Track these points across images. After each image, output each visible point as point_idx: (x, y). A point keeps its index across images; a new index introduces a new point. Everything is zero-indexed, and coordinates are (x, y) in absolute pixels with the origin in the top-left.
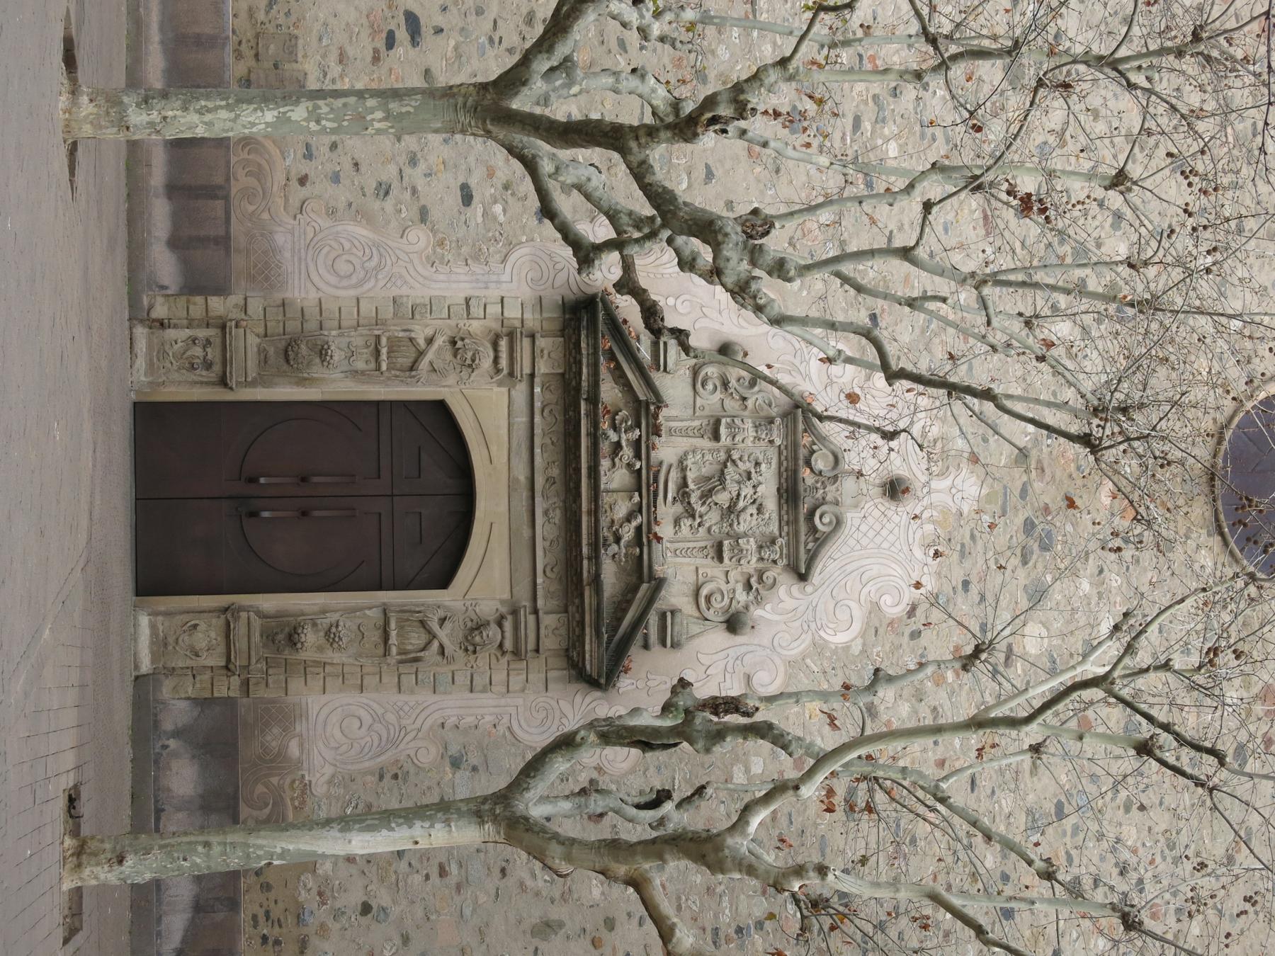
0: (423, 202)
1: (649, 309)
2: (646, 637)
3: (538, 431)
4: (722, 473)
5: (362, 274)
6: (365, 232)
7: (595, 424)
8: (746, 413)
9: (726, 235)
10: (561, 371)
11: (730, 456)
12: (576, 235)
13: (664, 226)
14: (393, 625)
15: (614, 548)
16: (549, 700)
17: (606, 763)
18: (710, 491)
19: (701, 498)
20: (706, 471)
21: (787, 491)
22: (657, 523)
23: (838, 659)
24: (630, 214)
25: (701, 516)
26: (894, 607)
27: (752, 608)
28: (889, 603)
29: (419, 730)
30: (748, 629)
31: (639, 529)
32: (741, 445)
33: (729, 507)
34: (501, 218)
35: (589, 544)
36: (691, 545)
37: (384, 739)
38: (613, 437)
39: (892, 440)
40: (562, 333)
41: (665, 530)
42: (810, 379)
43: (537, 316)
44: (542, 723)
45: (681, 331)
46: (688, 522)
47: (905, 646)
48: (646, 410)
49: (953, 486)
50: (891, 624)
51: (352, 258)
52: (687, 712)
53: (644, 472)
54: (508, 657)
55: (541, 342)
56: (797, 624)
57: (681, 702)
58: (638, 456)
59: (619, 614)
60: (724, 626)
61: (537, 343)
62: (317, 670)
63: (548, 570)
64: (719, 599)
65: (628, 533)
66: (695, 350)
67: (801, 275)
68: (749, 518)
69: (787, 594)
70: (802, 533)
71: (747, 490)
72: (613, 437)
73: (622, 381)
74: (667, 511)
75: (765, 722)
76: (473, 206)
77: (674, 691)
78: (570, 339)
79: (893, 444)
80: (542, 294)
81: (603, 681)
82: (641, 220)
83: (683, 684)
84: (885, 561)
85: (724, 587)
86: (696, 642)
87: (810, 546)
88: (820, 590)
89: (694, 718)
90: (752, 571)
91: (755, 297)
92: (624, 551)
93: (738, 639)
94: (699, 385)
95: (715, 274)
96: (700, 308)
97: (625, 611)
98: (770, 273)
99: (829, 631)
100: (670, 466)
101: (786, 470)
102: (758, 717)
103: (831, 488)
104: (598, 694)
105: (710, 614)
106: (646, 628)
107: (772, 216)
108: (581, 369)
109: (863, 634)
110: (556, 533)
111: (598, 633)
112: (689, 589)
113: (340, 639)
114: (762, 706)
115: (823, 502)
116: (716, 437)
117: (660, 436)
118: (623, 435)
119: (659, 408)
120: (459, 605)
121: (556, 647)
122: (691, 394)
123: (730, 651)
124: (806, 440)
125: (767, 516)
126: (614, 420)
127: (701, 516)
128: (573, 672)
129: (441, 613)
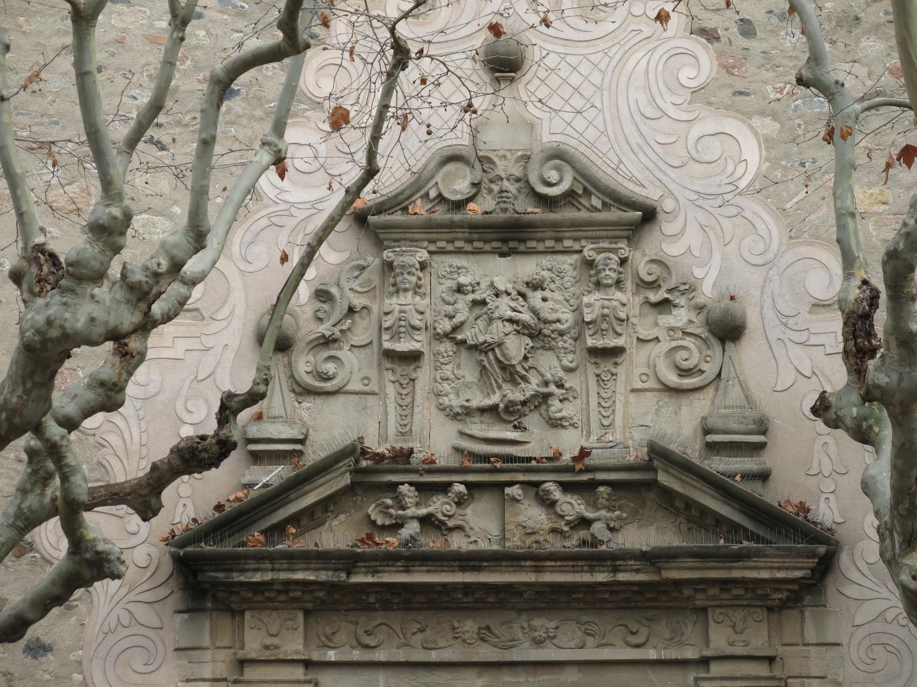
1: (185, 461)
2: (748, 476)
3: (401, 656)
4: (474, 348)
7: (390, 559)
8: (375, 308)
9: (49, 322)
10: (301, 616)
11: (446, 335)
12: (53, 583)
13: (38, 430)
15: (598, 528)
18: (504, 367)
19: (516, 384)
20: (470, 374)
21: (505, 241)
22: (557, 456)
23: (787, 156)
24: (23, 491)
25: (546, 384)
26: (701, 65)
27: (700, 300)
28: (693, 73)
30: (735, 307)
31: (566, 487)
32: (429, 317)
33: (531, 336)
35: (592, 570)
36: (594, 400)
38: (412, 528)
39: (408, 51)
40: (236, 613)
41: (568, 443)
43: (208, 655)
45: (223, 407)
46: (555, 404)
47: (764, 46)
48: (369, 473)
50: (728, 69)
52: (867, 398)
53: (471, 478)
55: (253, 645)
56: (725, 223)
57: (852, 411)
58: (444, 488)
59: (710, 521)
60: (729, 345)
61: (253, 655)
63: (631, 639)
65: (572, 506)
66: (255, 383)
67: (119, 196)
68: (549, 304)
69: (679, 242)
70: (577, 215)
71: (504, 307)
72: (412, 528)
73: (318, 514)
74: (537, 440)
75: (884, 264)
77: (834, 424)
78: (246, 600)
79: (414, 49)
80: (170, 649)
81: (822, 549)
82: (34, 472)
83: (822, 408)
84: (623, 79)
85: (665, 346)
86: (756, 393)
87: (596, 202)
88: (672, 186)
89: (877, 386)
90: (639, 300)
91: (157, 275)
92: (603, 512)
93: (753, 322)
94: (328, 386)
95: (127, 345)
96: (184, 376)
97: (704, 511)
98: (117, 250)
99: (738, 174)
100: (462, 434)
101: (471, 241)
102: (878, 281)
103: (502, 168)
104: (844, 558)
105: (711, 370)
106: (732, 476)
107: (25, 248)
108: (297, 582)
109: (746, 115)
110: (573, 625)
111: (740, 556)
112: (669, 404)
114: (861, 274)
115: (523, 180)
116: (414, 357)
117: (411, 451)
118: (410, 512)
119: (364, 452)
121: (764, 627)
122: (341, 398)
123: (773, 335)
124: (420, 208)
125: (546, 274)
126: (383, 528)
127: (546, 384)
128: (808, 599)
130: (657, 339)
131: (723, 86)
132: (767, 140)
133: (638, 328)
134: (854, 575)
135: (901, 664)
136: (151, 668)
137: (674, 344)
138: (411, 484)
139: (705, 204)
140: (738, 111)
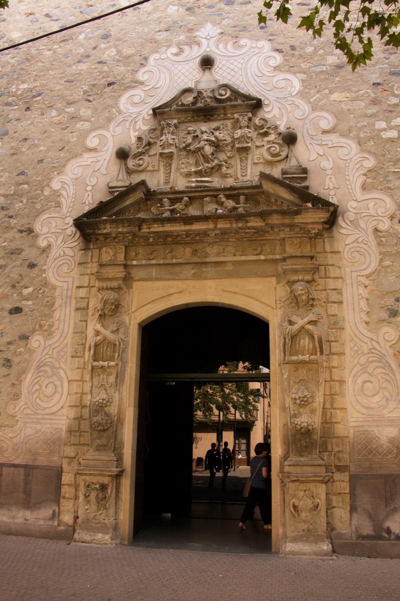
0: (17, 338)
5: (55, 377)
6: (30, 375)
14: (294, 358)
16: (346, 250)
17: (387, 214)
19: (208, 162)
23: (310, 85)
29: (372, 339)
31: (228, 197)
33: (216, 147)
34: (31, 289)
37: (379, 364)
41: (230, 182)
42: (141, 111)
43: (90, 265)
44: (362, 254)
46: (224, 169)
47: (300, 53)
49: (206, 38)
51: (45, 384)
54: (316, 276)
56: (289, 107)
58: (179, 200)
60: (292, 147)
62: (328, 414)
64: (274, 149)
65: (230, 204)
68: (222, 135)
69: (271, 113)
74: (216, 182)
76: (22, 307)
81: (332, 209)
85: (266, 147)
88: (267, 96)
94: (140, 168)
105: (284, 154)
109: (294, 73)
113: (305, 397)
120: (280, 312)
123: (308, 143)
129: (286, 324)
130: (263, 146)
131: (285, 65)
132: (302, 80)
133: (256, 142)
134: (343, 225)
135: (365, 259)
136: (70, 271)
137: (270, 146)
138: (168, 198)
139: (280, 101)
140: (291, 72)
